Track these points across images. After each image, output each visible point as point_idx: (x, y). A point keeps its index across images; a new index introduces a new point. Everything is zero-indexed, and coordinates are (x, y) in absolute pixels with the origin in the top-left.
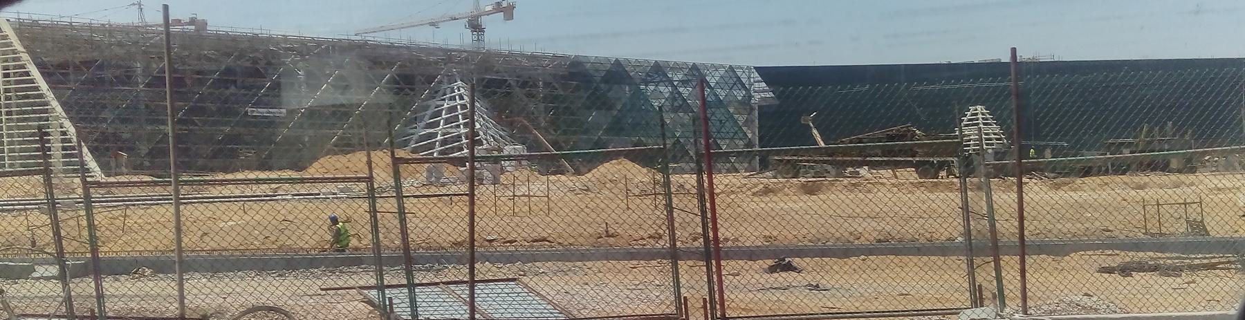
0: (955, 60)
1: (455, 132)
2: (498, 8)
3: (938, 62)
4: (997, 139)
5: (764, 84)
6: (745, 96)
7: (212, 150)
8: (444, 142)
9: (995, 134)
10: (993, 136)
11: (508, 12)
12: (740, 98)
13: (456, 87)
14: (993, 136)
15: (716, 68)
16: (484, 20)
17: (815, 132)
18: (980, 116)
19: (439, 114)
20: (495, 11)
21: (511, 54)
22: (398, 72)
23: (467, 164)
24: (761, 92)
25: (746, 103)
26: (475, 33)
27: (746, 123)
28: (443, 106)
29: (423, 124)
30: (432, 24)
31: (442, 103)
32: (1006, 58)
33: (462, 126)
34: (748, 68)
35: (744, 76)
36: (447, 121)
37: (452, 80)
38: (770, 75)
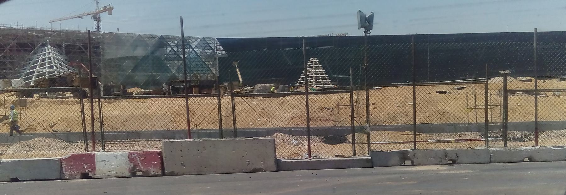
0: (510, 31)
1: (44, 71)
2: (105, 9)
3: (309, 36)
4: (321, 74)
5: (221, 47)
6: (211, 53)
7: (152, 75)
8: (38, 76)
9: (320, 72)
10: (319, 73)
11: (109, 10)
12: (208, 54)
13: (47, 49)
14: (319, 73)
15: (196, 39)
16: (101, 15)
17: (238, 70)
18: (314, 63)
19: (37, 62)
20: (104, 11)
21: (79, 32)
22: (16, 42)
23: (467, 75)
24: (220, 52)
25: (212, 57)
26: (96, 21)
27: (213, 65)
28: (39, 58)
29: (28, 67)
30: (80, 17)
31: (39, 57)
32: (533, 31)
33: (47, 68)
34: (214, 39)
35: (211, 42)
36: (41, 65)
37: (44, 45)
38: (226, 43)
